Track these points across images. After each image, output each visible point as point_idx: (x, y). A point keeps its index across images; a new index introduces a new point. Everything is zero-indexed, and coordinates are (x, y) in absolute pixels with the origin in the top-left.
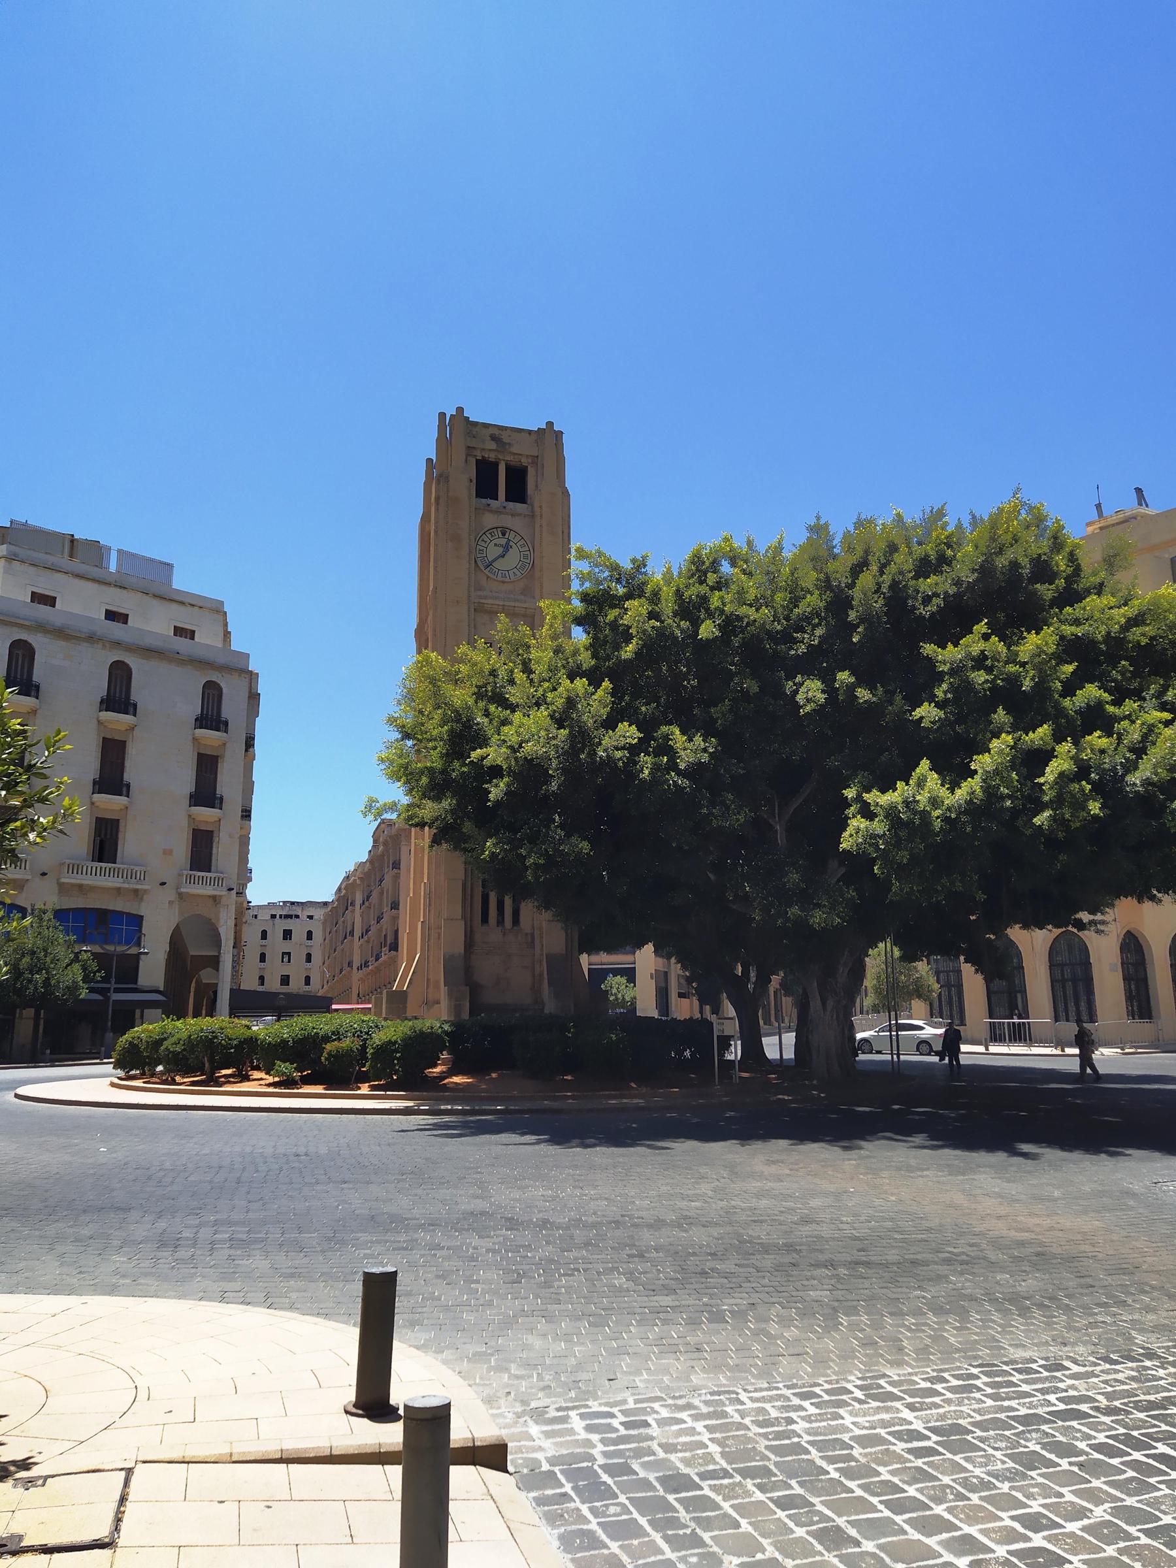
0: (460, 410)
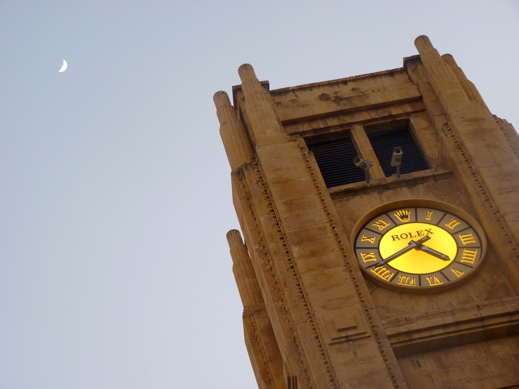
0: (246, 70)
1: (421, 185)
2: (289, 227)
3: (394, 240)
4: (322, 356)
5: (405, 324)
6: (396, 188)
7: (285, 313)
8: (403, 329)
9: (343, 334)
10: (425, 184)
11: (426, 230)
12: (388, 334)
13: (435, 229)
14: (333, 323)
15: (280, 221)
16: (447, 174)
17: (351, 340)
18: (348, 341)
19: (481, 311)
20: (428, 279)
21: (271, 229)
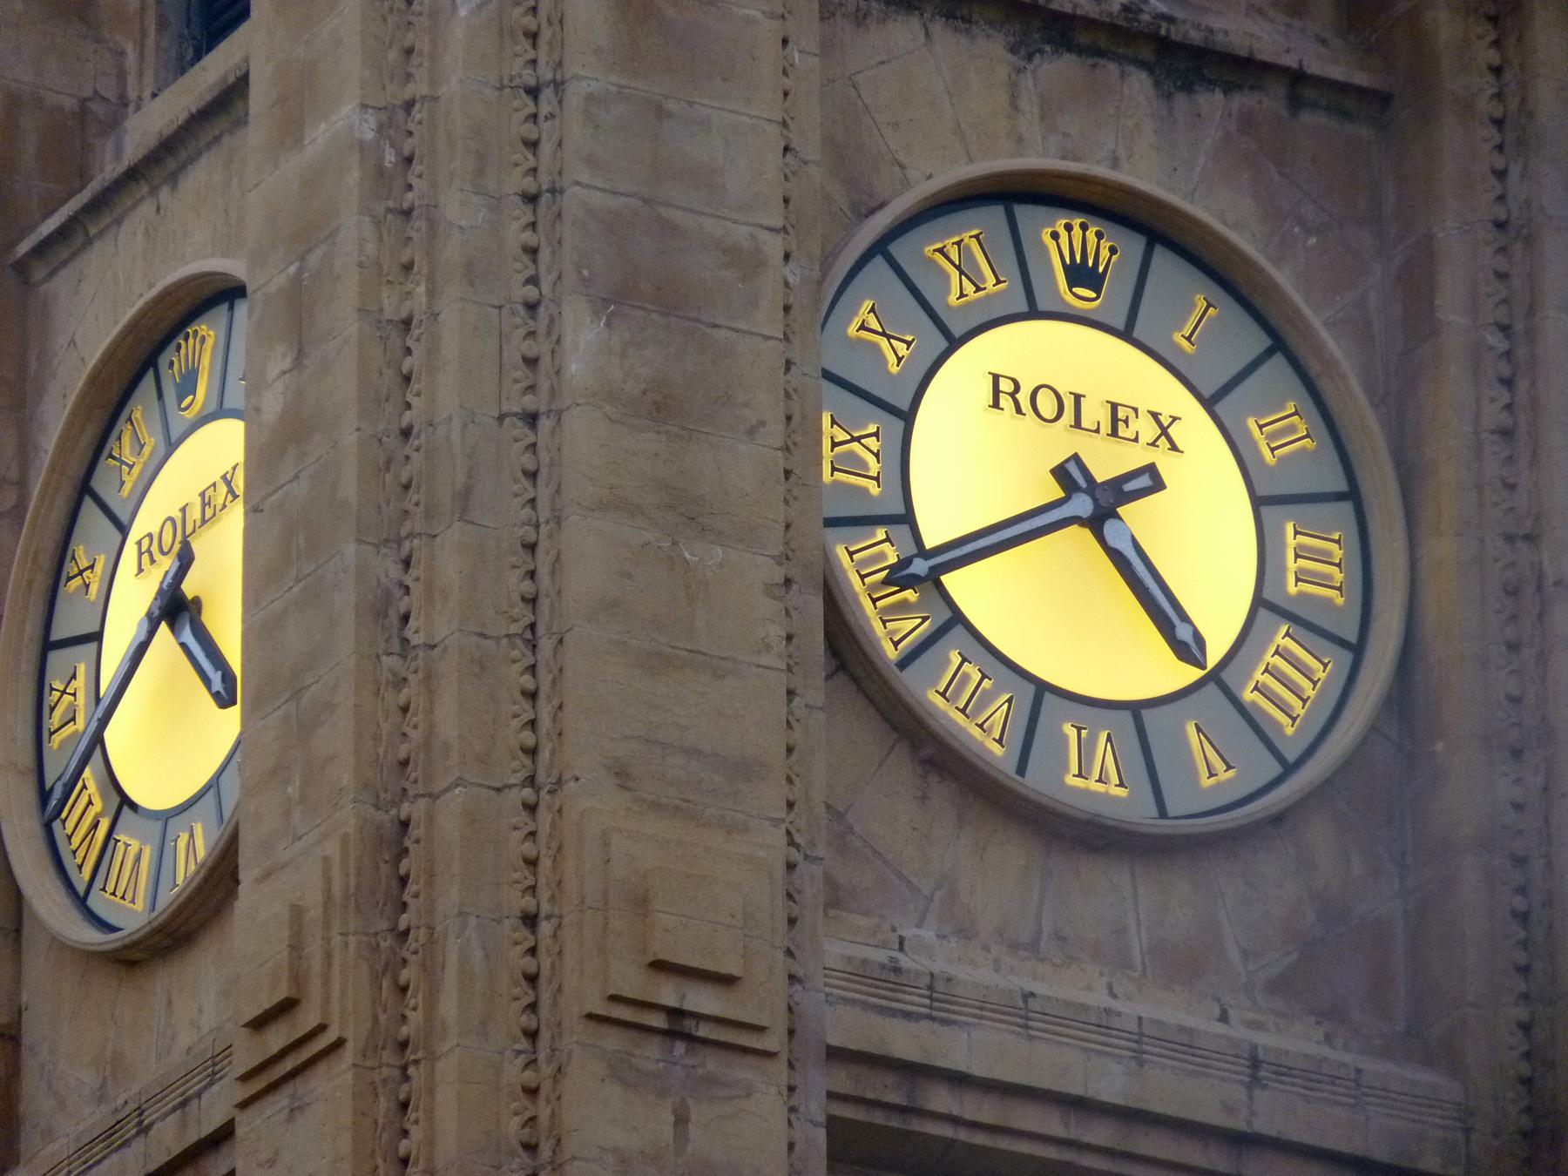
1: (1219, 95)
2: (592, 162)
3: (996, 404)
4: (524, 1044)
5: (919, 1017)
6: (1100, 53)
7: (396, 647)
8: (903, 1041)
9: (668, 993)
10: (1240, 101)
11: (1155, 416)
12: (835, 1040)
13: (1196, 427)
14: (642, 903)
15: (558, 85)
16: (1360, 92)
17: (690, 1038)
18: (670, 1034)
19: (1258, 1093)
20: (1071, 732)
21: (490, 93)
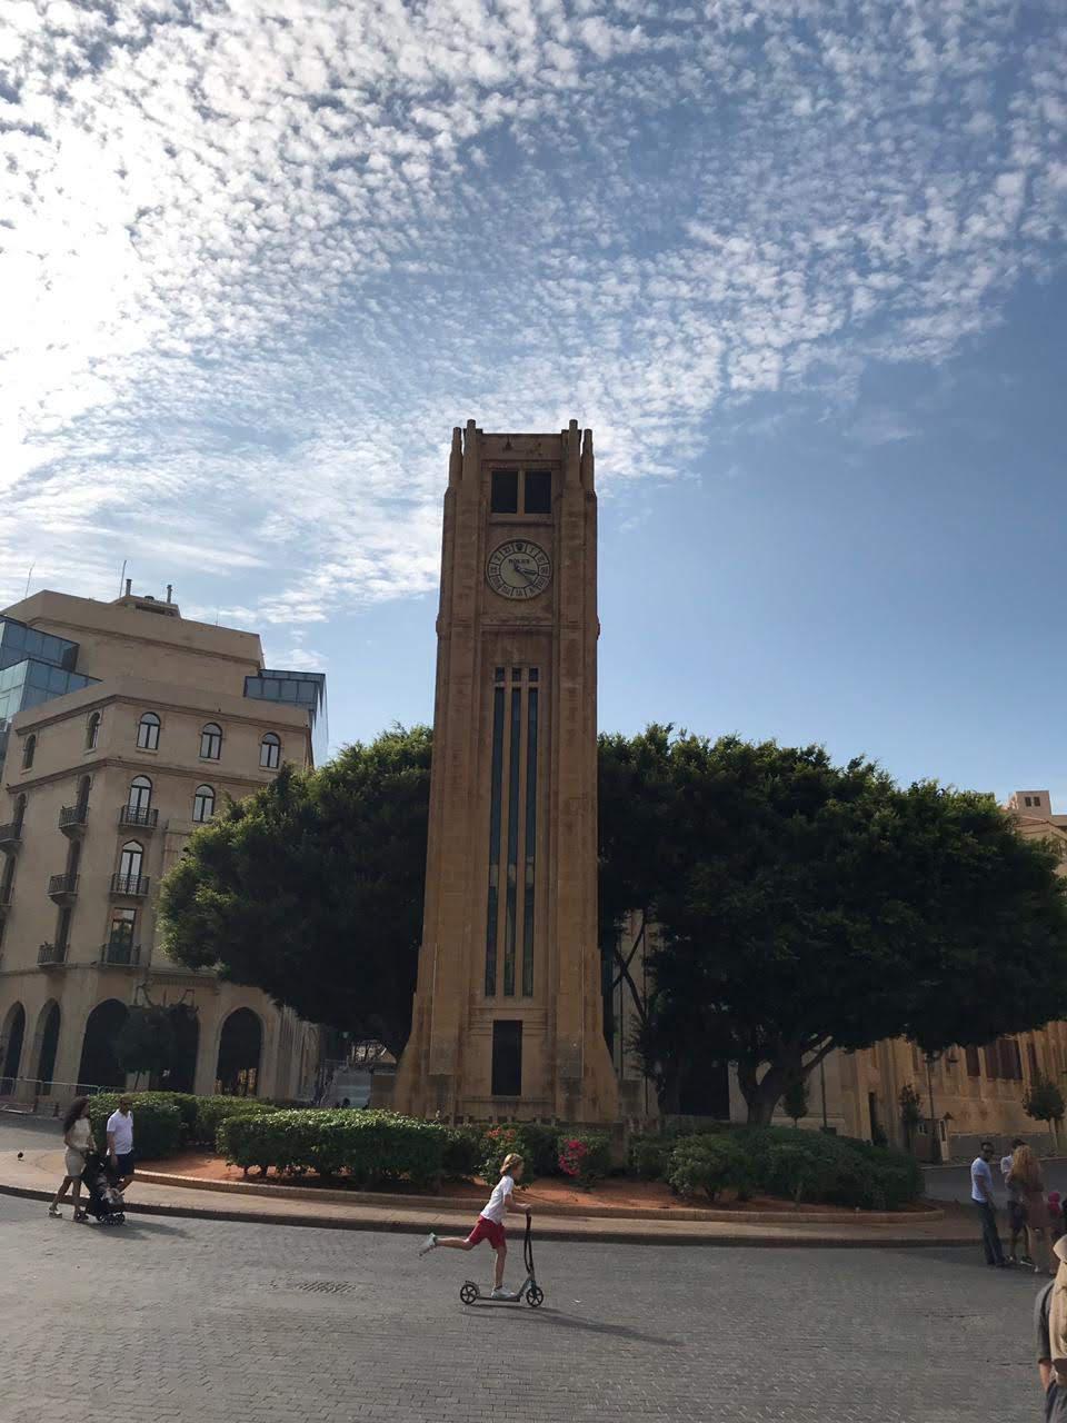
0: (472, 423)
